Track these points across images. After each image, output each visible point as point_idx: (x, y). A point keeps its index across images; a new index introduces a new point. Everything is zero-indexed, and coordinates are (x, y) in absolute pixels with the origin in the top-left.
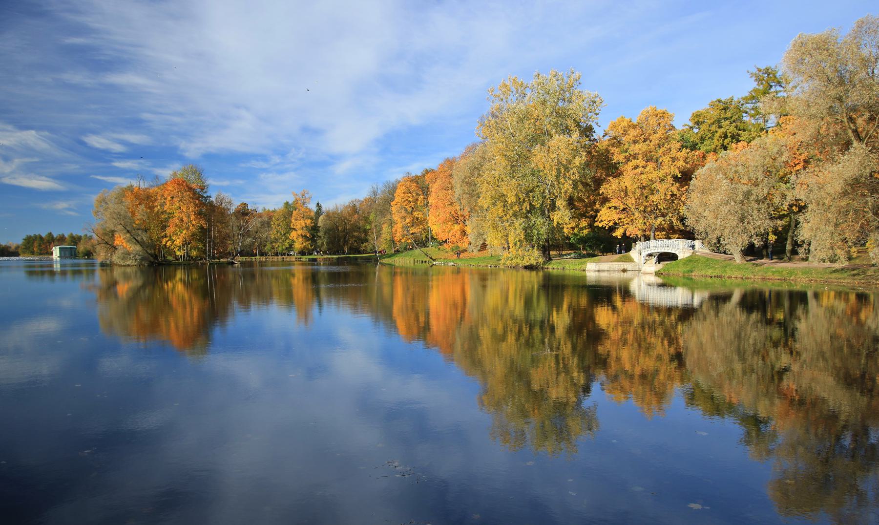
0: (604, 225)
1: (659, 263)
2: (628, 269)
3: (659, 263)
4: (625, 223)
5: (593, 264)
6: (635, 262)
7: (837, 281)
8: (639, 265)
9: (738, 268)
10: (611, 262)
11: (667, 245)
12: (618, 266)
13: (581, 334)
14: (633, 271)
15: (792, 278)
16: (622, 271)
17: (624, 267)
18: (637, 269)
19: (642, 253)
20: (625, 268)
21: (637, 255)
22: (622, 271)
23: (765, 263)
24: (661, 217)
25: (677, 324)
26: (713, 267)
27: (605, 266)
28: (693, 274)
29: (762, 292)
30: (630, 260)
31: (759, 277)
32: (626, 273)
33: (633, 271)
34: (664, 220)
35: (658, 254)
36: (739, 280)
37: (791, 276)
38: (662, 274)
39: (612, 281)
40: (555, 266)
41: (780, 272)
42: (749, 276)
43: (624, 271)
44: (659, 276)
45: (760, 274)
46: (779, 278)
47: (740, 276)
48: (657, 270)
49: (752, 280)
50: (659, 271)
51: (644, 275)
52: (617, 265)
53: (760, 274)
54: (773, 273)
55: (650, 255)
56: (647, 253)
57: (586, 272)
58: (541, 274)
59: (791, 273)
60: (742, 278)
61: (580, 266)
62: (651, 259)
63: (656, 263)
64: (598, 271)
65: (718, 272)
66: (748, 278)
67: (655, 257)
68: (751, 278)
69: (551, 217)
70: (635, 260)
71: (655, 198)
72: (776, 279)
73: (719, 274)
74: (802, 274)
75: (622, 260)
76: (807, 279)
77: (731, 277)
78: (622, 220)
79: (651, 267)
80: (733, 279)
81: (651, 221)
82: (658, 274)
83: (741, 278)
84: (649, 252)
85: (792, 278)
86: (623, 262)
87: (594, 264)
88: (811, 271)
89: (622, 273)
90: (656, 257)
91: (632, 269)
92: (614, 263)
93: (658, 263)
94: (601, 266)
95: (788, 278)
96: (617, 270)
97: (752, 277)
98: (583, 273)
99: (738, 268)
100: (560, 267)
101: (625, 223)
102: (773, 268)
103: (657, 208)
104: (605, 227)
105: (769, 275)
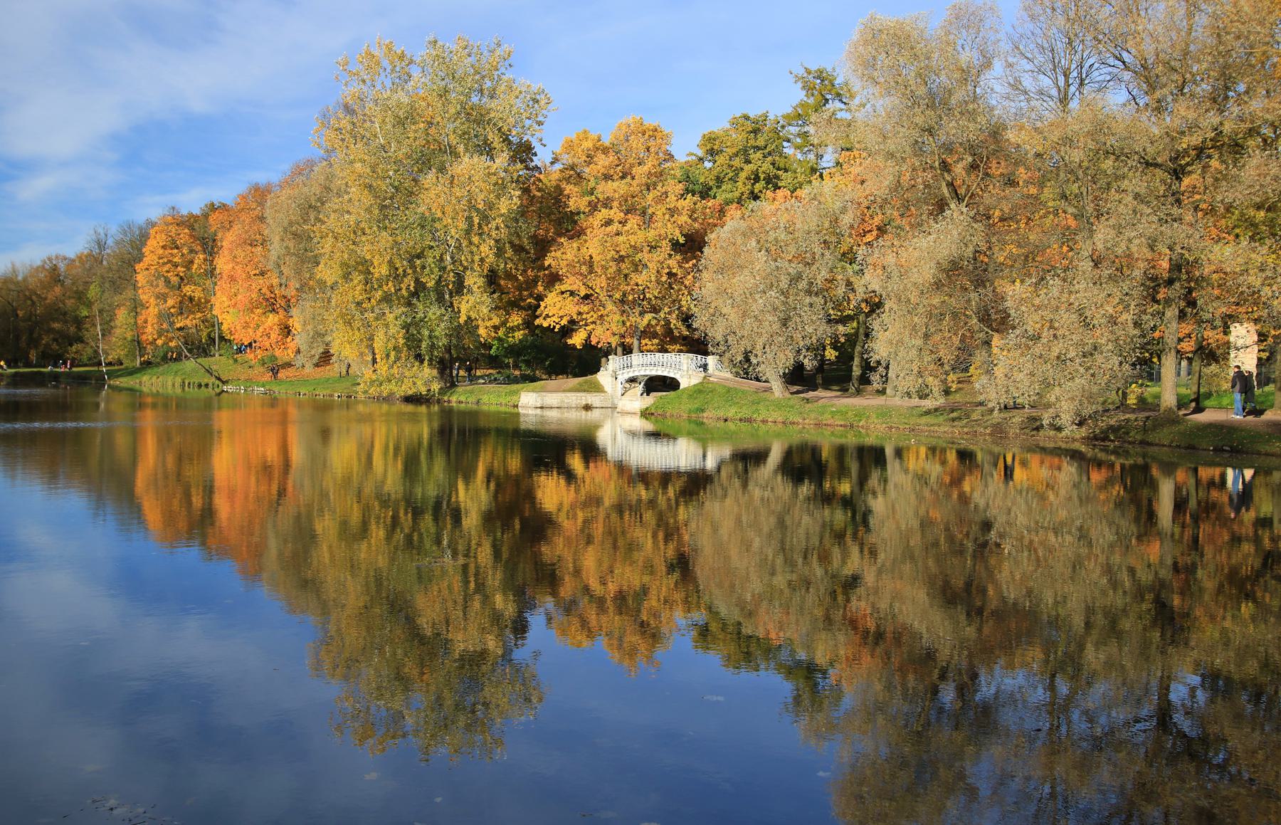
1: (648, 395)
2: (595, 406)
3: (648, 395)
5: (531, 394)
9: (778, 405)
10: (564, 391)
16: (583, 408)
19: (619, 377)
22: (583, 408)
28: (705, 415)
30: (598, 388)
31: (811, 422)
36: (780, 426)
37: (861, 420)
38: (652, 414)
41: (843, 414)
43: (587, 408)
44: (647, 419)
45: (813, 416)
46: (842, 423)
47: (780, 419)
49: (800, 426)
50: (647, 409)
55: (632, 380)
56: (627, 376)
59: (859, 415)
63: (642, 395)
64: (542, 408)
65: (746, 412)
66: (794, 423)
67: (640, 383)
68: (798, 424)
70: (606, 389)
71: (641, 279)
72: (837, 425)
77: (767, 421)
78: (584, 316)
79: (634, 403)
82: (646, 414)
90: (642, 384)
92: (569, 394)
96: (574, 406)
97: (801, 421)
99: (778, 405)
100: (472, 399)
104: (554, 327)
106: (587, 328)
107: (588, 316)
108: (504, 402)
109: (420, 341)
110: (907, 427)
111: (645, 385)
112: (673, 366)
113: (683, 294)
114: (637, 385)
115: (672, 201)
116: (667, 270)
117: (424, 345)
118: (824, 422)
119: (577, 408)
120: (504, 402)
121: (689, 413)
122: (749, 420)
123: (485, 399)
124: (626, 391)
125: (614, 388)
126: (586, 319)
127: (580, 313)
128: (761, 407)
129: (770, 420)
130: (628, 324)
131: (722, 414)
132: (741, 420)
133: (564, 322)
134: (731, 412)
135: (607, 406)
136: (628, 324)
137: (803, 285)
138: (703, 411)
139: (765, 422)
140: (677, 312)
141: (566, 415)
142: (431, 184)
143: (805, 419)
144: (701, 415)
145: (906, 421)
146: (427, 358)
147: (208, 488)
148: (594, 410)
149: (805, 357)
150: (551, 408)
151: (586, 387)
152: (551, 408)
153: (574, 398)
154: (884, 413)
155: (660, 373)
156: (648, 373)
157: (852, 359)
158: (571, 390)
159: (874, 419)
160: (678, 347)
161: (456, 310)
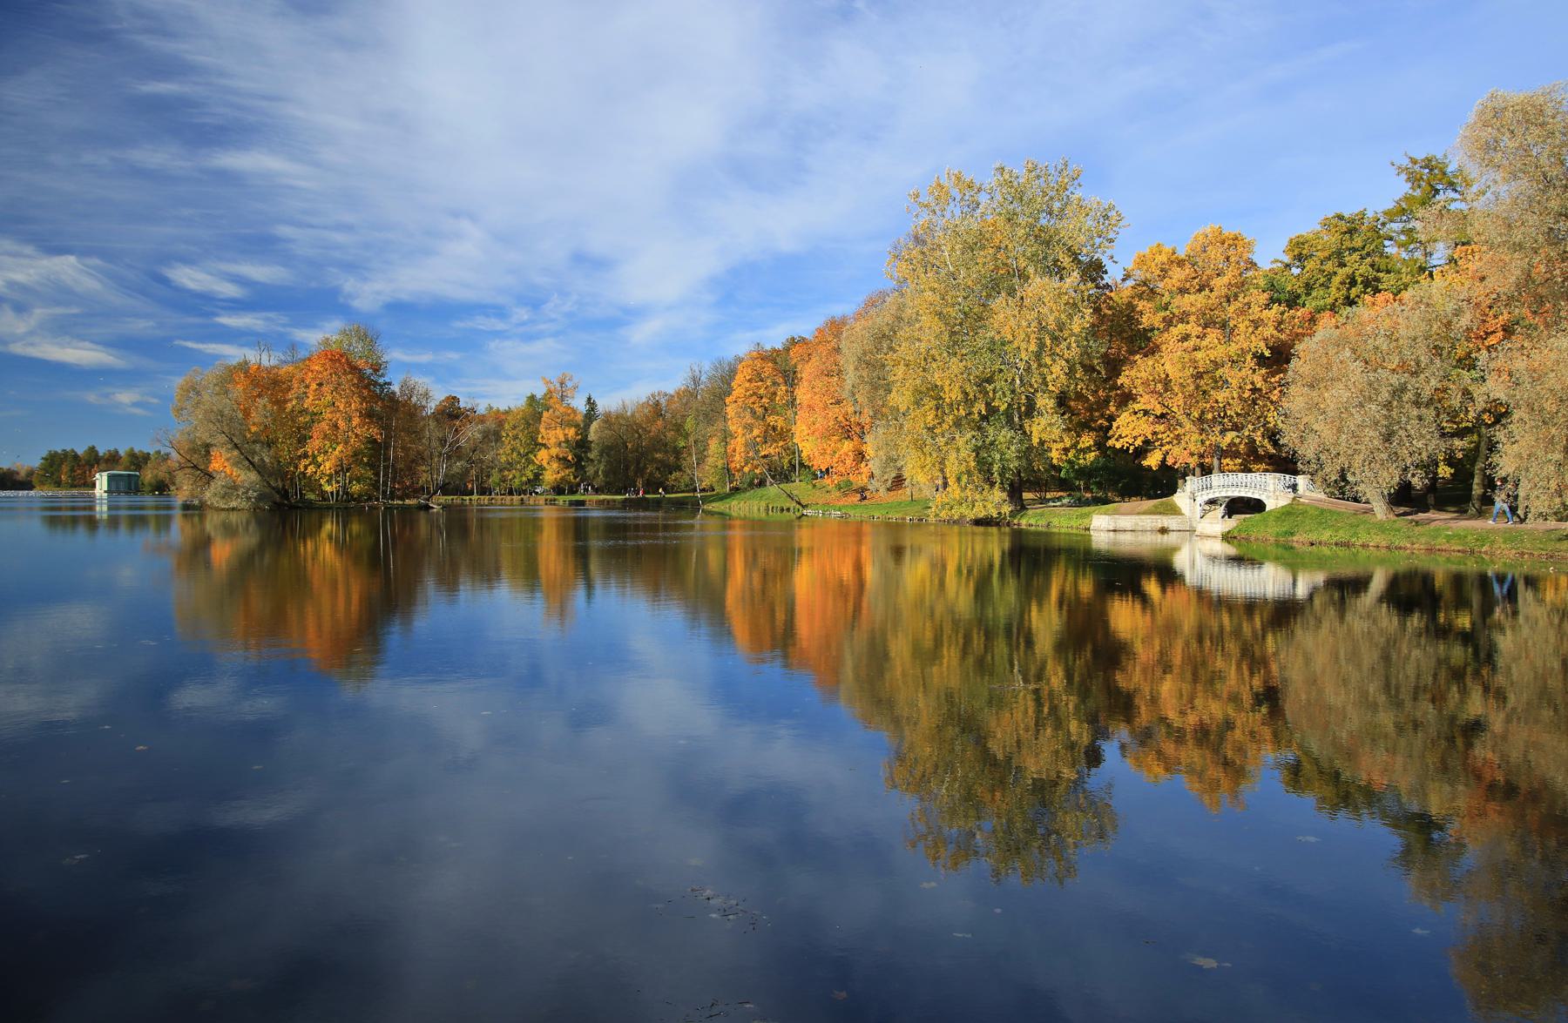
0: (1126, 445)
1: (1230, 517)
3: (1230, 517)
4: (1164, 441)
6: (1183, 514)
8: (1191, 521)
9: (1381, 528)
10: (1139, 514)
14: (1180, 531)
15: (1484, 549)
16: (1159, 531)
19: (1198, 499)
22: (1159, 531)
24: (1232, 430)
27: (1125, 522)
28: (1295, 538)
30: (1174, 511)
31: (1422, 547)
32: (1166, 535)
33: (1180, 531)
35: (1227, 500)
38: (1235, 537)
41: (1462, 538)
42: (1402, 544)
43: (1163, 531)
44: (1229, 542)
45: (1423, 540)
46: (1460, 548)
47: (1384, 544)
48: (1227, 530)
49: (1408, 551)
50: (1229, 532)
53: (1423, 540)
55: (1212, 502)
56: (1206, 498)
59: (1482, 539)
60: (1388, 548)
61: (1080, 522)
62: (1215, 509)
63: (1223, 517)
64: (1114, 531)
65: (1342, 536)
66: (1400, 548)
67: (1221, 505)
68: (1405, 549)
70: (1183, 511)
72: (1454, 551)
74: (1505, 542)
77: (1368, 546)
78: (1160, 436)
79: (1214, 525)
80: (1371, 548)
81: (1213, 439)
86: (1160, 514)
89: (1159, 536)
90: (1223, 506)
91: (1179, 529)
92: (1143, 517)
94: (1120, 521)
95: (1476, 549)
96: (1149, 529)
97: (1409, 545)
99: (1381, 528)
101: (1164, 441)
103: (1225, 414)
104: (1128, 448)
111: (1226, 507)
118: (1437, 547)
119: (1152, 531)
122: (1347, 545)
123: (1055, 521)
126: (1162, 439)
132: (1336, 544)
134: (1326, 535)
135: (1184, 529)
138: (1292, 534)
141: (1140, 538)
144: (1290, 539)
149: (1413, 475)
151: (1162, 510)
156: (1230, 494)
157: (1472, 476)
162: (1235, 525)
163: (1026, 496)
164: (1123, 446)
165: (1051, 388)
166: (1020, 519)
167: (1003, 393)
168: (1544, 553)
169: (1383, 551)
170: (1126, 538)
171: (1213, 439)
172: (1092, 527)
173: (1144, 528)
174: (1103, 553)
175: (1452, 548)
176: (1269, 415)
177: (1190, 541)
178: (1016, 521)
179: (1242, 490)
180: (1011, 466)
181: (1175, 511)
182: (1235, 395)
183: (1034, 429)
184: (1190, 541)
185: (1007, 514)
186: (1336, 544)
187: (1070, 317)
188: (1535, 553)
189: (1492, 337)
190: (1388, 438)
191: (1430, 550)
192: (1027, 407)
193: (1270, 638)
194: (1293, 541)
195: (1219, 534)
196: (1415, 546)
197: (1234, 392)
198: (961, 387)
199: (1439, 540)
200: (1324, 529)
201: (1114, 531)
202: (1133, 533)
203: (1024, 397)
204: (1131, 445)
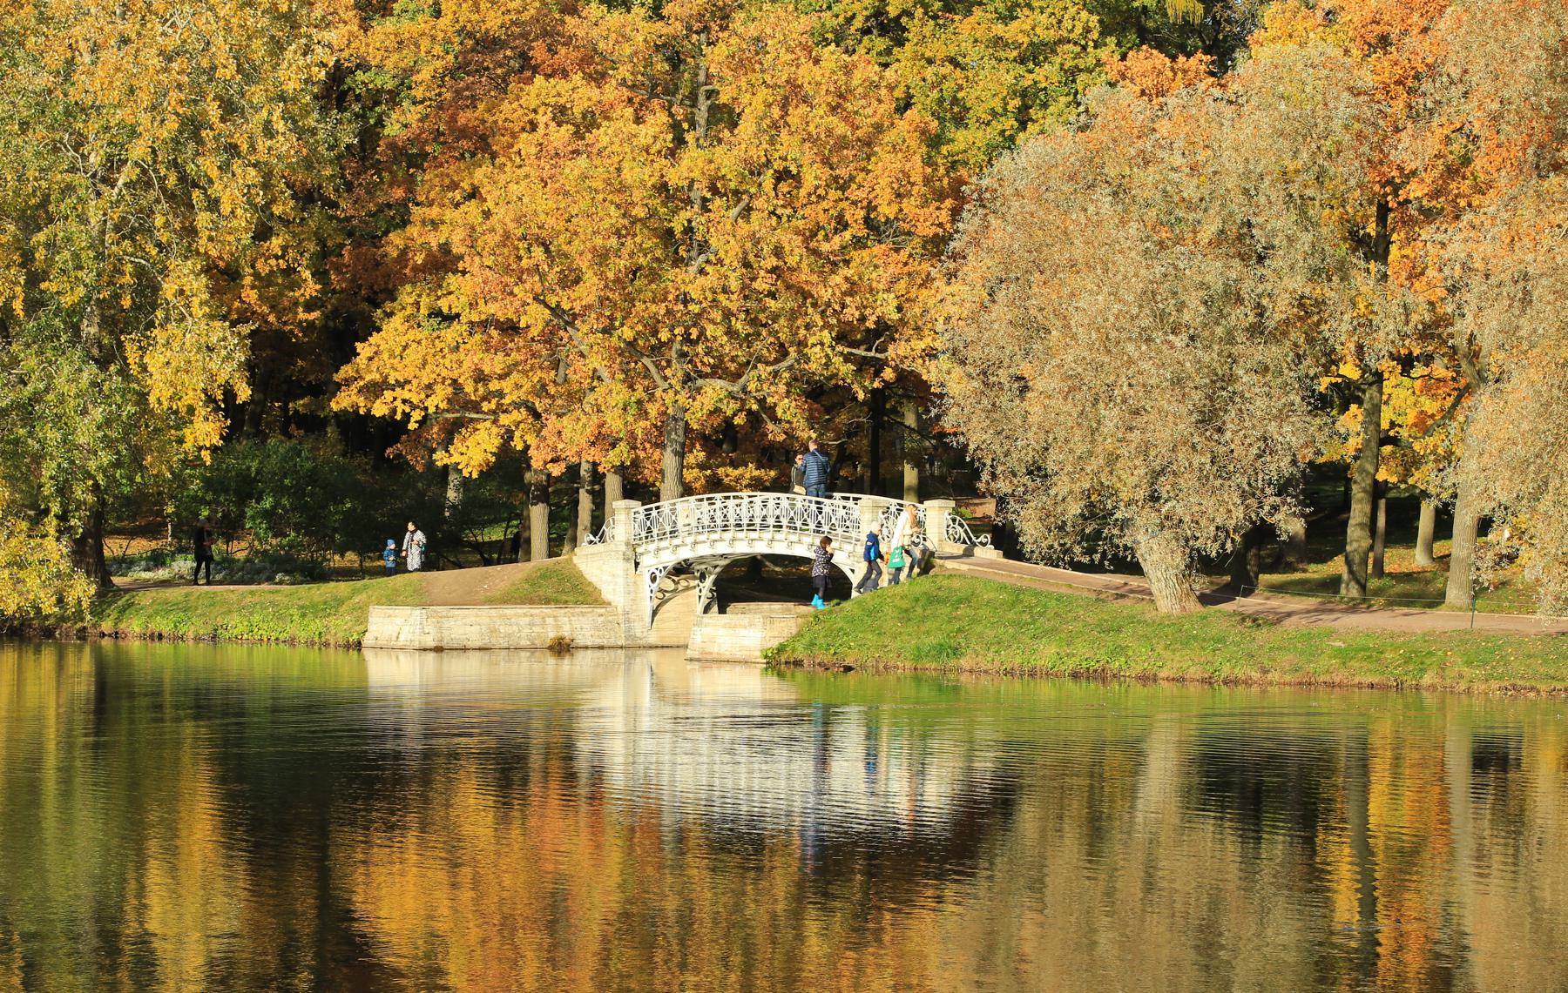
0: (401, 407)
1: (722, 611)
2: (580, 641)
3: (722, 611)
4: (506, 401)
5: (406, 610)
6: (607, 604)
7: (1041, 783)
8: (628, 621)
9: (1177, 635)
10: (491, 602)
11: (771, 521)
12: (531, 625)
13: (796, 878)
14: (601, 648)
15: (1427, 679)
16: (551, 648)
17: (558, 627)
18: (621, 642)
19: (644, 561)
20: (566, 633)
21: (621, 567)
22: (551, 648)
23: (1289, 615)
24: (713, 375)
25: (796, 915)
26: (1054, 630)
27: (467, 625)
28: (964, 662)
29: (1205, 756)
30: (581, 593)
31: (1288, 678)
32: (567, 660)
33: (601, 648)
34: (731, 396)
35: (724, 562)
36: (1193, 689)
37: (1423, 671)
38: (798, 663)
39: (398, 697)
40: (163, 625)
41: (1373, 655)
42: (1239, 673)
43: (562, 648)
44: (780, 675)
45: (1285, 659)
46: (1375, 679)
47: (1194, 672)
48: (775, 644)
49: (1255, 689)
50: (781, 649)
51: (703, 668)
52: (524, 621)
53: (1285, 659)
54: (1344, 656)
55: (681, 570)
56: (671, 559)
57: (367, 653)
58: (82, 666)
59: (1416, 657)
60: (1208, 681)
61: (316, 626)
62: (687, 588)
63: (707, 610)
64: (439, 650)
65: (1083, 654)
66: (1236, 682)
67: (702, 577)
68: (1248, 682)
69: (132, 357)
70: (607, 595)
71: (692, 281)
72: (1360, 686)
73: (1094, 665)
74: (1469, 664)
75: (541, 592)
76: (1494, 685)
77: (1155, 679)
78: (494, 385)
79: (742, 632)
80: (1165, 684)
81: (669, 397)
82: (778, 663)
83: (1203, 681)
84: (685, 554)
85: (1427, 679)
86: (548, 602)
87: (417, 612)
88: (1500, 648)
89: (551, 661)
90: (709, 581)
91: (598, 642)
92: (509, 611)
93: (715, 608)
94: (451, 623)
95: (1410, 681)
96: (525, 643)
97: (1256, 675)
98: (342, 663)
99: (1177, 635)
100: (194, 627)
101: (506, 401)
102: (1330, 634)
103: (702, 333)
104: (407, 416)
105: (1325, 666)
106: (505, 419)
107: (507, 385)
108: (302, 635)
109: (38, 459)
110: (1559, 685)
111: (715, 583)
112: (785, 522)
113: (808, 327)
114: (693, 583)
115: (780, 64)
116: (772, 262)
117: (48, 470)
118: (1322, 679)
119: (533, 649)
120: (302, 635)
121: (918, 658)
122: (1100, 676)
123: (236, 624)
124: (664, 602)
125: (631, 591)
126: (500, 394)
127: (480, 377)
128: (1125, 638)
129: (1163, 674)
130: (653, 410)
131: (1018, 660)
132: (1075, 676)
133: (437, 401)
134: (1046, 654)
135: (612, 642)
136: (653, 410)
137: (1241, 316)
138: (956, 651)
139: (1146, 679)
140: (786, 375)
141: (502, 667)
142: (359, 74)
143: (1265, 672)
144: (952, 663)
145: (1552, 672)
146: (55, 508)
147: (583, 791)
148: (580, 655)
149: (1275, 508)
150: (465, 649)
151: (550, 592)
152: (465, 649)
153: (524, 621)
154: (1483, 652)
155: (780, 549)
156: (722, 548)
157: (1347, 507)
158: (507, 599)
159: (1457, 665)
160: (751, 471)
161: (134, 370)
162: (794, 631)
163: (113, 547)
164: (394, 411)
165: (202, 243)
166: (118, 620)
167: (76, 256)
168: (1559, 685)
169: (1192, 689)
170: (465, 673)
171: (669, 397)
172: (368, 640)
173: (513, 643)
174: (373, 713)
175: (1356, 681)
176: (812, 340)
177: (628, 670)
178: (107, 626)
179: (778, 536)
180: (92, 465)
181: (583, 593)
182: (734, 285)
183: (154, 361)
184: (628, 670)
185: (85, 605)
186: (1075, 676)
187: (277, 47)
188: (1542, 687)
189: (854, 22)
190: (1209, 419)
191: (1307, 685)
192: (138, 291)
193: (812, 927)
194: (960, 670)
195: (757, 655)
196: (1270, 676)
197: (733, 276)
198: (1220, 430)
199: (1324, 662)
200: (1034, 637)
201: (439, 650)
202: (486, 656)
203: (129, 268)
204: (414, 407)
